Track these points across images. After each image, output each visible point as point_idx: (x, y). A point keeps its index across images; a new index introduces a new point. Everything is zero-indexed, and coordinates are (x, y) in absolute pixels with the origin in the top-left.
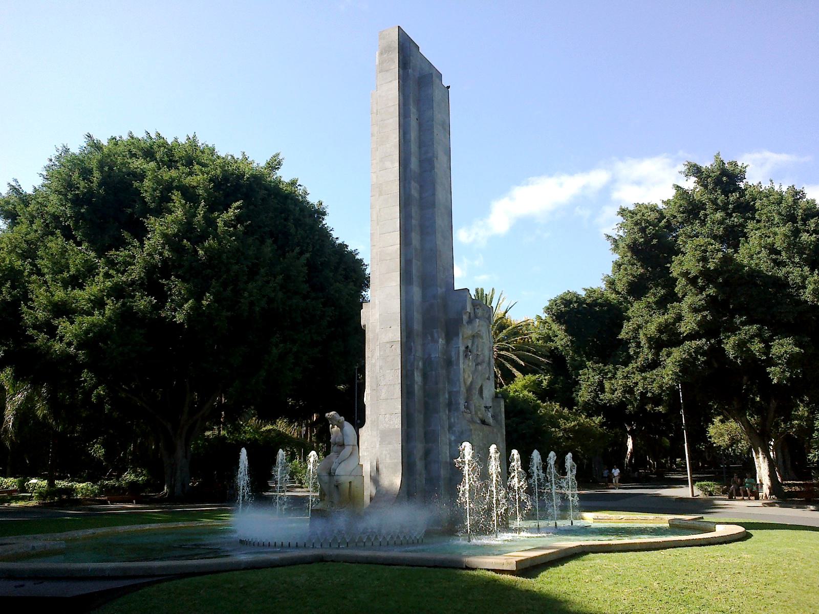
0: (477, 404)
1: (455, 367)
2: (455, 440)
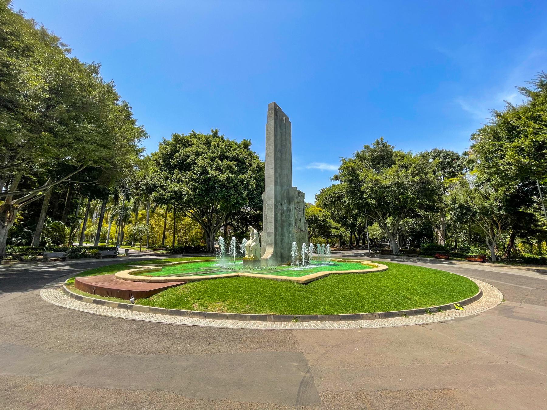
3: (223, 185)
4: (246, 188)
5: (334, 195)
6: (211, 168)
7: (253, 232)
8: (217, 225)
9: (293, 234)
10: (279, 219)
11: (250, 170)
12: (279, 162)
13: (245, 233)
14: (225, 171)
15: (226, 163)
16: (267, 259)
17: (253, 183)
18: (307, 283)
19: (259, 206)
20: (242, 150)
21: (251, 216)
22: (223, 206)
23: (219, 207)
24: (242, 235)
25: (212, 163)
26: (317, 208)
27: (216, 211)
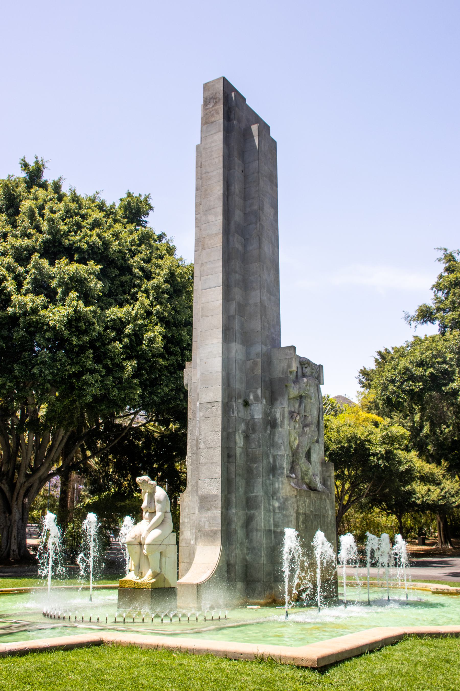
0: (304, 469)
1: (280, 429)
2: (279, 507)
3: (58, 341)
4: (132, 351)
5: (419, 372)
6: (19, 285)
7: (152, 495)
8: (35, 470)
9: (286, 499)
10: (238, 451)
11: (146, 291)
12: (236, 264)
13: (130, 496)
14: (66, 294)
15: (66, 268)
16: (198, 587)
17: (155, 333)
18: (324, 666)
19: (174, 407)
20: (118, 227)
21: (148, 436)
22: (59, 407)
23: (43, 411)
24: (119, 506)
25: (21, 269)
26: (364, 414)
27: (34, 425)
